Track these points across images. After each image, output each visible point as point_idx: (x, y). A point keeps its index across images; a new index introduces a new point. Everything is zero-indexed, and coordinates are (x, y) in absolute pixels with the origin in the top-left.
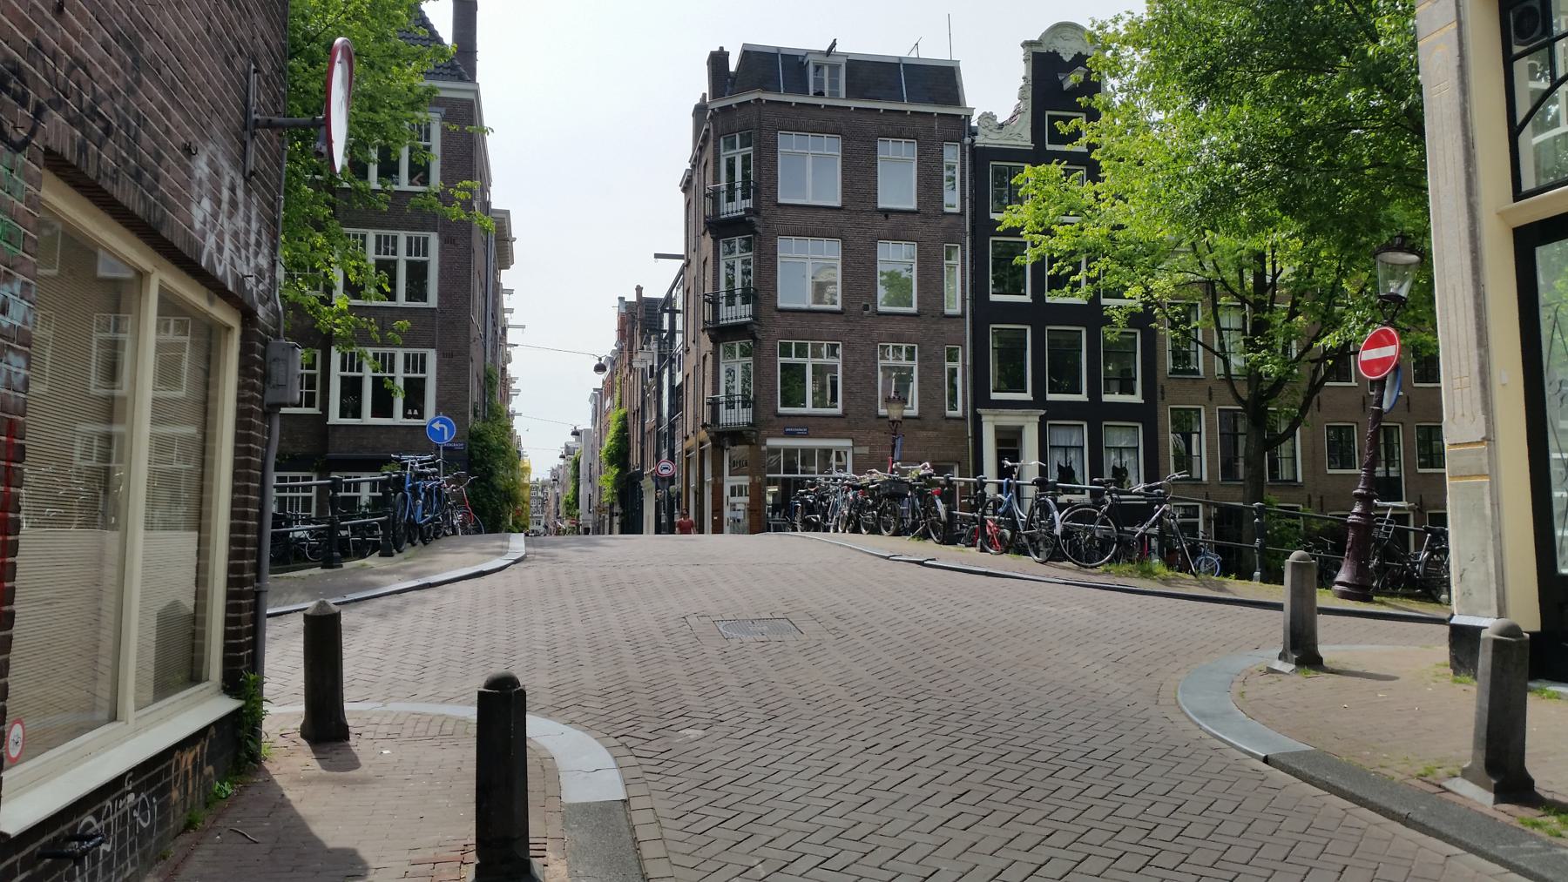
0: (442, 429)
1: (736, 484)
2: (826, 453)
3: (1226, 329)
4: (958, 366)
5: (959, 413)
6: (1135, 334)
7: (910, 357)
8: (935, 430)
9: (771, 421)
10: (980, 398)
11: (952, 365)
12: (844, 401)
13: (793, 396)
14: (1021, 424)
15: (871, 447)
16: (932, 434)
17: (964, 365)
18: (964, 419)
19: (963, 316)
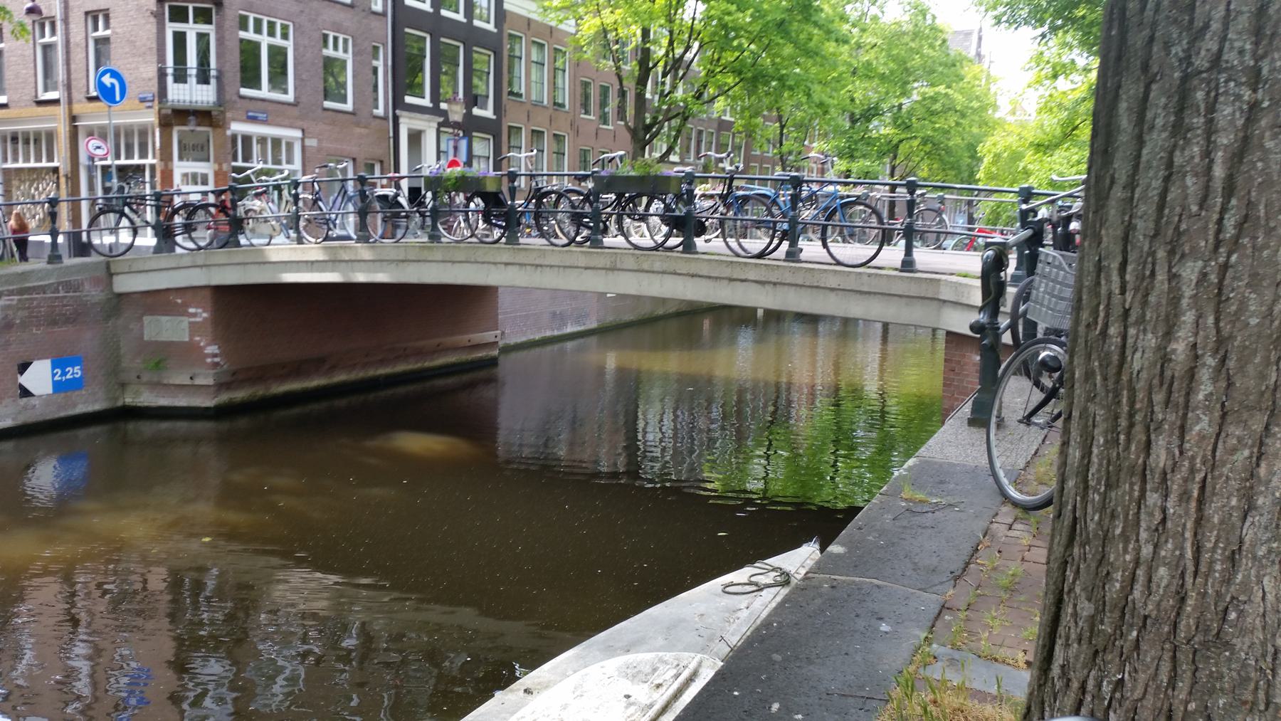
0: (113, 85)
1: (190, 170)
2: (277, 142)
3: (1068, 286)
4: (379, 64)
5: (380, 111)
6: (489, 56)
7: (285, 36)
8: (365, 127)
9: (235, 102)
10: (398, 103)
11: (179, 27)
12: (296, 88)
13: (251, 79)
14: (419, 128)
15: (319, 141)
16: (363, 131)
17: (385, 65)
18: (385, 118)
19: (384, 14)
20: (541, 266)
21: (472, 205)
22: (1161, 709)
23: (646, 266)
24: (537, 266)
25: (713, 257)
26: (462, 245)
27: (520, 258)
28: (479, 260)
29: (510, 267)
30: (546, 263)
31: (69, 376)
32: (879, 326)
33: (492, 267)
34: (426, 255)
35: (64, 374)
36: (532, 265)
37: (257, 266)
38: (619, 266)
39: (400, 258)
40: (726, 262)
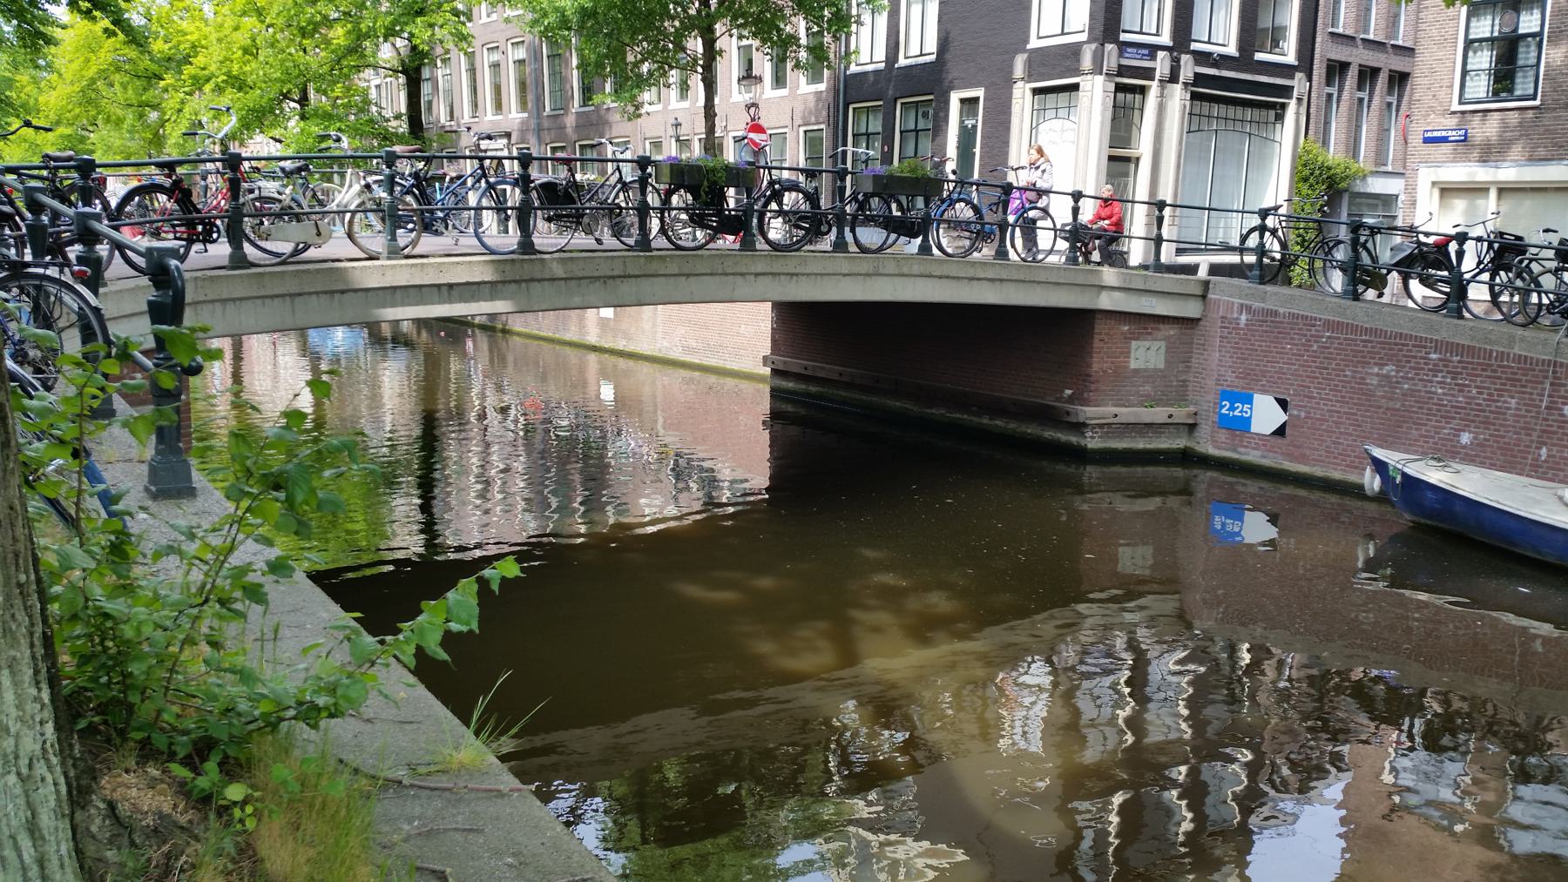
20: (797, 275)
21: (1498, 280)
22: (1312, 299)
23: (905, 270)
24: (792, 275)
25: (318, 266)
26: (700, 252)
27: (655, 267)
28: (729, 270)
29: (761, 278)
30: (808, 271)
31: (1237, 413)
32: (1120, 96)
33: (739, 279)
34: (830, 267)
35: (1232, 409)
36: (325, 293)
37: (126, 320)
38: (881, 271)
39: (616, 273)
40: (128, 290)
